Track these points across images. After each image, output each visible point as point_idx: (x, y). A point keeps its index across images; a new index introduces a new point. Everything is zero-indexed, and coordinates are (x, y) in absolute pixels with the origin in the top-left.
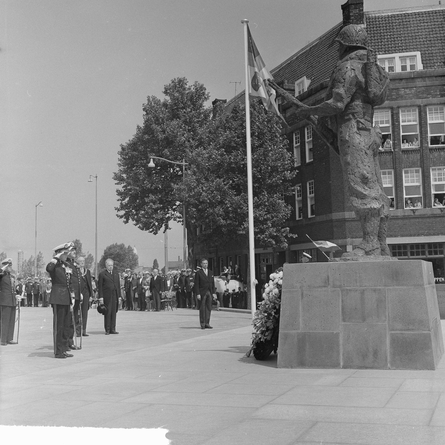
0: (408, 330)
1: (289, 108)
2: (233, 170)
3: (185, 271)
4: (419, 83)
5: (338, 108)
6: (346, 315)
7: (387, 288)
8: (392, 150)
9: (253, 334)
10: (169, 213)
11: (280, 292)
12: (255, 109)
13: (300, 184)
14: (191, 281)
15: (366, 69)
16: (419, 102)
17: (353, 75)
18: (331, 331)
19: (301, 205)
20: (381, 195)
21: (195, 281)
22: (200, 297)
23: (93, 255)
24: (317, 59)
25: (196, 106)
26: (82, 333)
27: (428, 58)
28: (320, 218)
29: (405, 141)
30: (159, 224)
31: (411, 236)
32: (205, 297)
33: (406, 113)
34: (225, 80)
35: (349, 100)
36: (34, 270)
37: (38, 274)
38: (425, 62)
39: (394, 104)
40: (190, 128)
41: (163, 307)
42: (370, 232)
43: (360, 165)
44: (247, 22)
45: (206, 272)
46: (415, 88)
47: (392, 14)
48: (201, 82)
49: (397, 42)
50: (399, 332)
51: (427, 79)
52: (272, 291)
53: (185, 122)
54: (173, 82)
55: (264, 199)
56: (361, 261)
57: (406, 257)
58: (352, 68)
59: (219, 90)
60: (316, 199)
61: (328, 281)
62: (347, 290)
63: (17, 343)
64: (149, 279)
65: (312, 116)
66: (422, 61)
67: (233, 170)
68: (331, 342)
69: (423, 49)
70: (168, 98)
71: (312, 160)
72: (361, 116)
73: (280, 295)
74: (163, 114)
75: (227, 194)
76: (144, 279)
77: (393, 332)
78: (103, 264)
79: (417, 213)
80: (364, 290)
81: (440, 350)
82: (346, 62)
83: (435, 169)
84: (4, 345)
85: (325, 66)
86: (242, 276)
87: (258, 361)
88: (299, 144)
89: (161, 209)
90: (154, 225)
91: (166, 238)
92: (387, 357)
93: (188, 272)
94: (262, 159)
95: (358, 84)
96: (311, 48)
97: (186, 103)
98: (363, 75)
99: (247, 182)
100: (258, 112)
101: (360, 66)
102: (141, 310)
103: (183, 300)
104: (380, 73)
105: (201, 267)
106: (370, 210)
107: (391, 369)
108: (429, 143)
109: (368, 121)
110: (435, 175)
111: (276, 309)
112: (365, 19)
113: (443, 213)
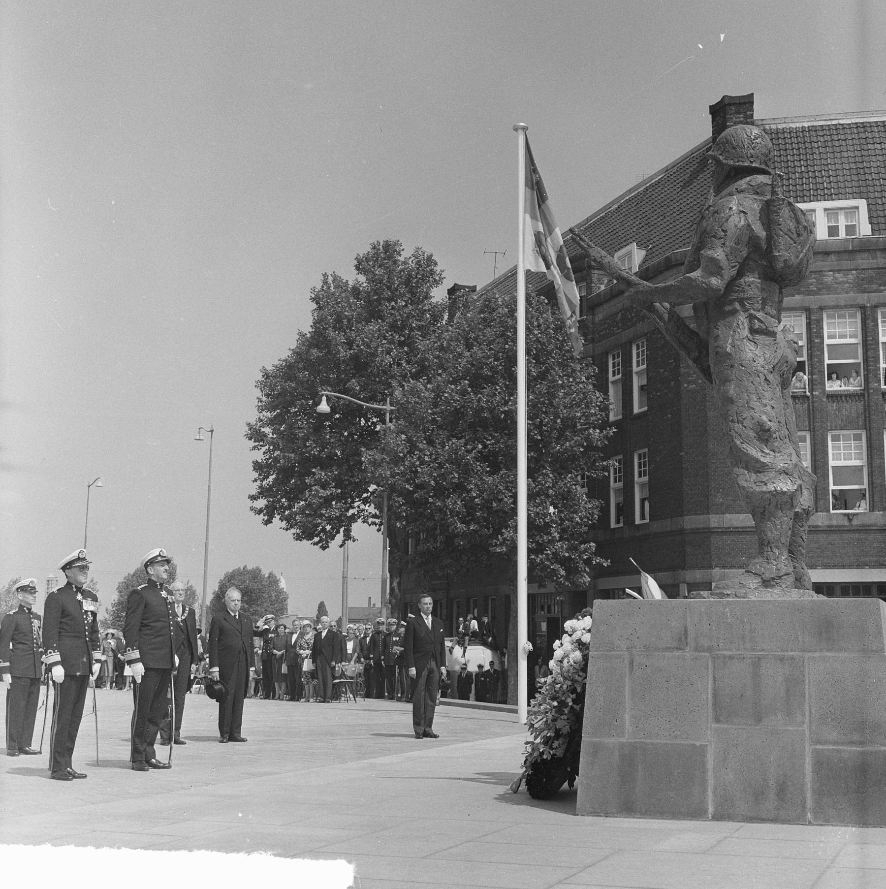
1: (600, 304)
2: (484, 424)
3: (383, 623)
5: (712, 289)
6: (722, 710)
8: (808, 394)
9: (527, 743)
11: (585, 658)
13: (621, 457)
14: (396, 643)
15: (768, 213)
17: (742, 223)
19: (621, 499)
21: (404, 643)
22: (415, 672)
24: (658, 210)
25: (418, 297)
26: (172, 738)
28: (667, 525)
29: (834, 376)
30: (332, 528)
31: (843, 567)
32: (425, 673)
33: (837, 320)
35: (734, 272)
39: (812, 301)
40: (403, 339)
41: (336, 693)
43: (755, 404)
44: (525, 129)
45: (428, 621)
46: (854, 272)
48: (428, 250)
49: (820, 180)
51: (879, 254)
52: (567, 656)
53: (393, 327)
54: (374, 248)
55: (546, 483)
56: (753, 598)
58: (740, 209)
59: (462, 267)
62: (724, 656)
63: (40, 753)
64: (310, 636)
66: (870, 217)
67: (484, 424)
69: (872, 195)
70: (362, 278)
71: (646, 408)
73: (586, 665)
74: (353, 309)
75: (473, 470)
76: (302, 635)
78: (220, 597)
79: (855, 522)
80: (759, 659)
82: (729, 198)
84: (13, 755)
86: (499, 638)
87: (536, 802)
89: (338, 498)
90: (324, 530)
91: (346, 558)
92: (804, 798)
93: (390, 624)
94: (543, 403)
95: (753, 241)
97: (396, 290)
98: (763, 225)
101: (757, 206)
102: (292, 699)
103: (377, 683)
106: (774, 495)
108: (882, 382)
111: (577, 693)
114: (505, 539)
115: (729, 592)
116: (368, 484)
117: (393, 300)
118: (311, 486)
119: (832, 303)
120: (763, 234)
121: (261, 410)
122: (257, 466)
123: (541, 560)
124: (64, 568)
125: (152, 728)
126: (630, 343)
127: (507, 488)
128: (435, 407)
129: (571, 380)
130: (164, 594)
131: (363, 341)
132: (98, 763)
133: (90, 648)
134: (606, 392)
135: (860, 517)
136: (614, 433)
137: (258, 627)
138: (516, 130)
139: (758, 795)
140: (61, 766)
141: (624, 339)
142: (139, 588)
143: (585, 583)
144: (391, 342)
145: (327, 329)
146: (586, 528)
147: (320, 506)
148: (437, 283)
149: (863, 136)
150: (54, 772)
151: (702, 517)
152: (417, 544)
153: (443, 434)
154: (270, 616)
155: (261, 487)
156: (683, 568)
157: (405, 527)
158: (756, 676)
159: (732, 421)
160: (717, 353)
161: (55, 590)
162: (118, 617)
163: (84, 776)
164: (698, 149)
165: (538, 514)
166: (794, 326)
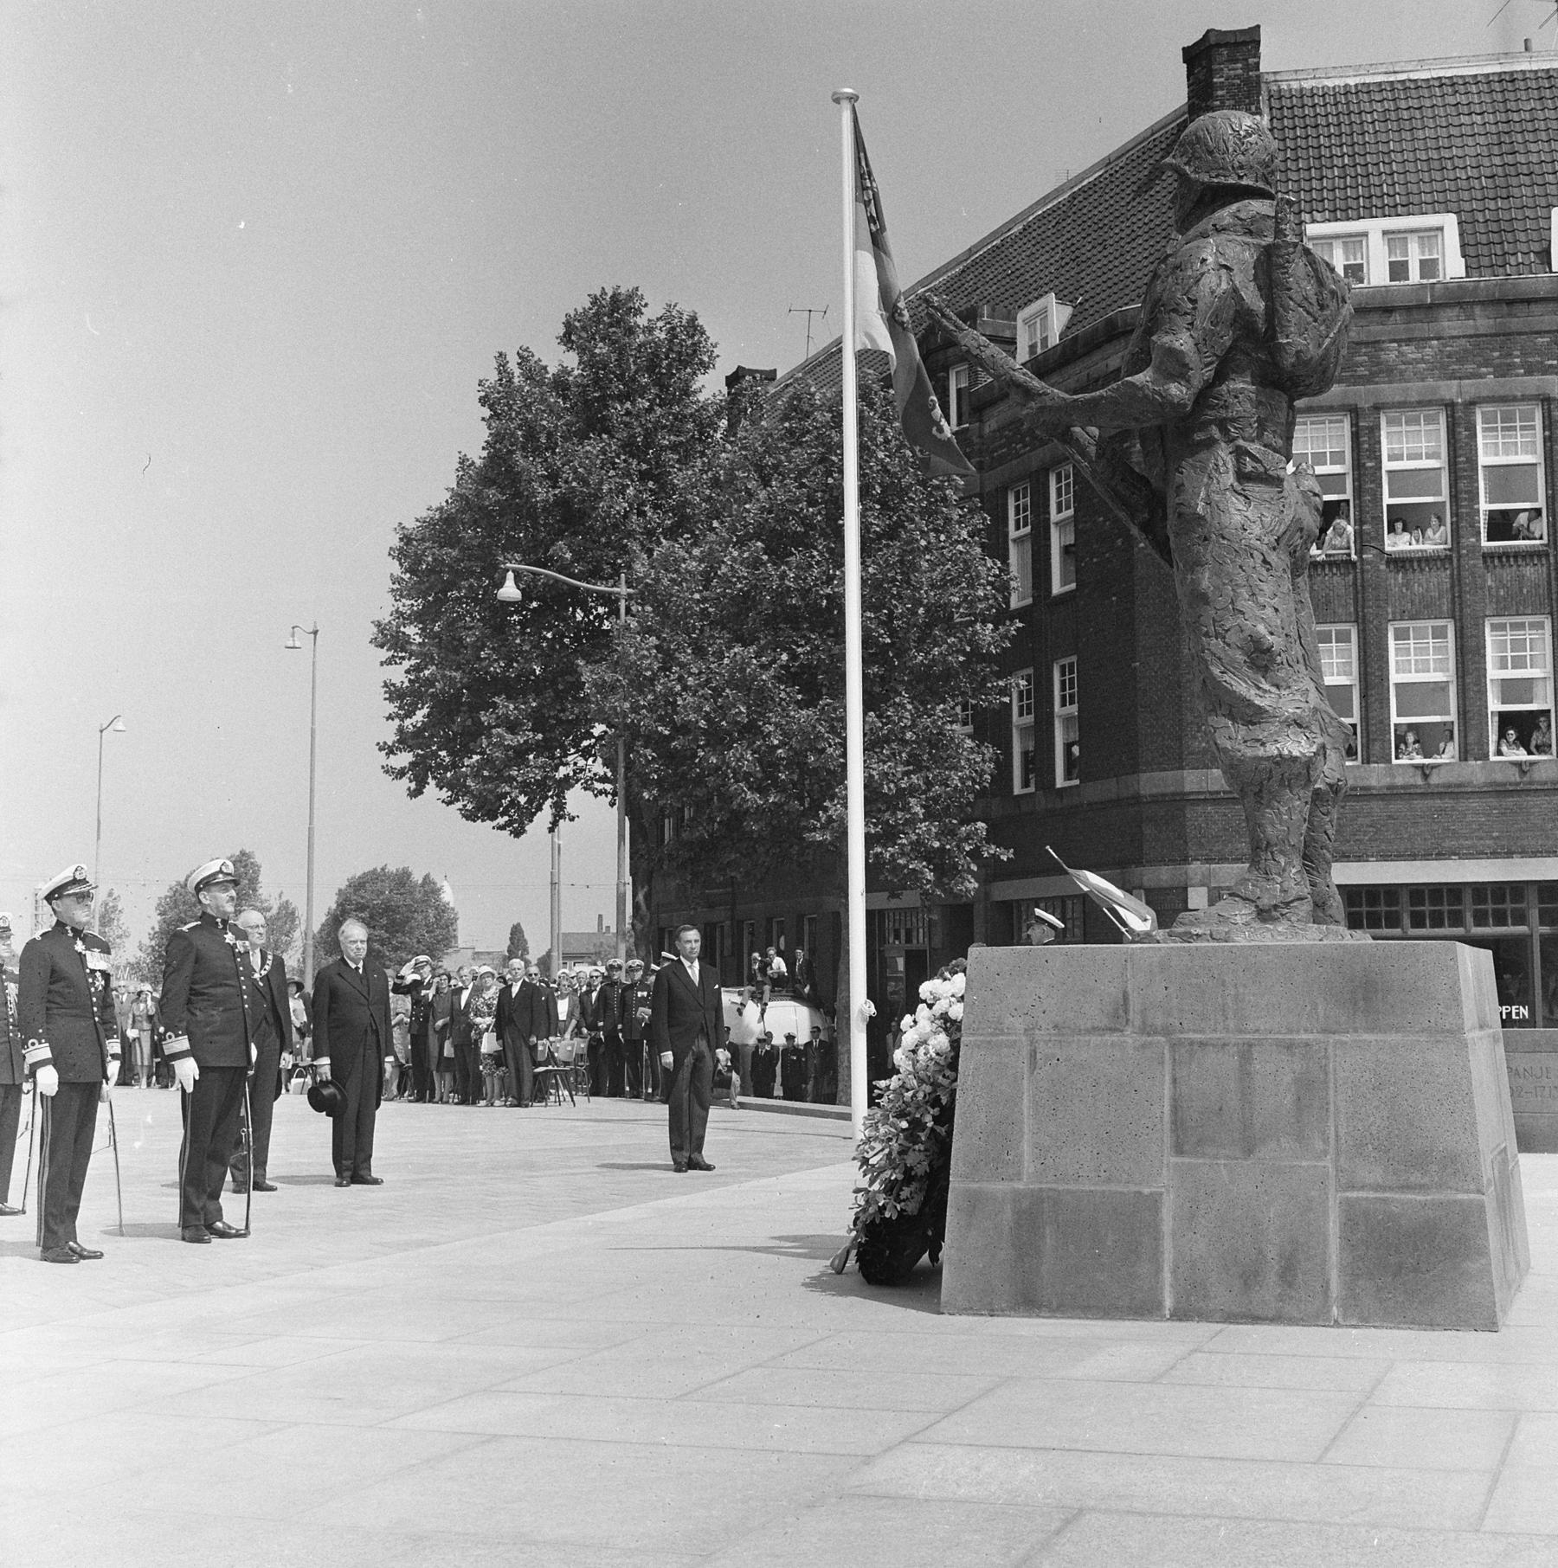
1: (992, 403)
2: (792, 618)
3: (620, 967)
4: (1451, 324)
5: (1171, 403)
6: (1186, 1135)
7: (1333, 1038)
9: (857, 1191)
10: (567, 764)
11: (955, 1045)
12: (871, 405)
13: (1030, 671)
14: (642, 1002)
15: (1269, 268)
16: (1450, 390)
17: (1224, 286)
18: (1133, 1188)
20: (1316, 710)
21: (653, 1002)
26: (254, 1181)
27: (1483, 239)
29: (1399, 526)
30: (530, 802)
31: (1414, 857)
33: (1404, 428)
35: (1209, 373)
38: (1471, 251)
39: (1362, 395)
40: (644, 466)
41: (540, 1090)
43: (1245, 604)
44: (853, 99)
45: (694, 970)
48: (686, 309)
50: (1372, 1195)
51: (1477, 310)
52: (925, 1042)
53: (629, 447)
56: (1241, 941)
57: (1397, 931)
58: (1220, 261)
60: (1085, 725)
61: (1126, 1012)
62: (1192, 1043)
63: (24, 1212)
64: (492, 993)
65: (1077, 429)
66: (1463, 246)
67: (792, 618)
68: (1134, 1221)
69: (1466, 206)
70: (572, 360)
71: (1073, 586)
72: (1251, 432)
73: (956, 1058)
75: (772, 699)
76: (478, 991)
78: (330, 938)
79: (1435, 779)
83: (1502, 627)
86: (819, 987)
87: (874, 1290)
88: (1028, 528)
89: (540, 749)
91: (556, 850)
93: (630, 970)
94: (894, 580)
95: (1242, 317)
96: (1074, 197)
98: (1260, 289)
100: (883, 416)
101: (1249, 256)
102: (463, 1102)
103: (611, 1070)
106: (1277, 763)
108: (1484, 535)
109: (1276, 451)
110: (1501, 646)
112: (1264, 97)
114: (830, 819)
115: (1200, 931)
116: (589, 724)
117: (628, 399)
118: (490, 727)
119: (1397, 398)
120: (1259, 305)
121: (398, 594)
122: (394, 693)
123: (892, 855)
124: (49, 898)
125: (215, 1169)
126: (1044, 471)
127: (832, 730)
128: (706, 588)
129: (943, 537)
130: (229, 938)
131: (575, 472)
132: (121, 1231)
133: (102, 1035)
134: (1005, 559)
135: (1443, 770)
136: (1018, 629)
137: (402, 978)
138: (837, 101)
140: (58, 1238)
141: (1035, 465)
142: (185, 928)
143: (968, 890)
146: (971, 797)
147: (508, 763)
148: (705, 366)
149: (1451, 100)
150: (46, 1248)
152: (677, 829)
153: (721, 638)
154: (422, 958)
155: (400, 730)
156: (1139, 863)
158: (1245, 1074)
160: (1180, 515)
161: (37, 936)
163: (98, 1256)
164: (1162, 125)
165: (887, 774)
166: (1320, 445)
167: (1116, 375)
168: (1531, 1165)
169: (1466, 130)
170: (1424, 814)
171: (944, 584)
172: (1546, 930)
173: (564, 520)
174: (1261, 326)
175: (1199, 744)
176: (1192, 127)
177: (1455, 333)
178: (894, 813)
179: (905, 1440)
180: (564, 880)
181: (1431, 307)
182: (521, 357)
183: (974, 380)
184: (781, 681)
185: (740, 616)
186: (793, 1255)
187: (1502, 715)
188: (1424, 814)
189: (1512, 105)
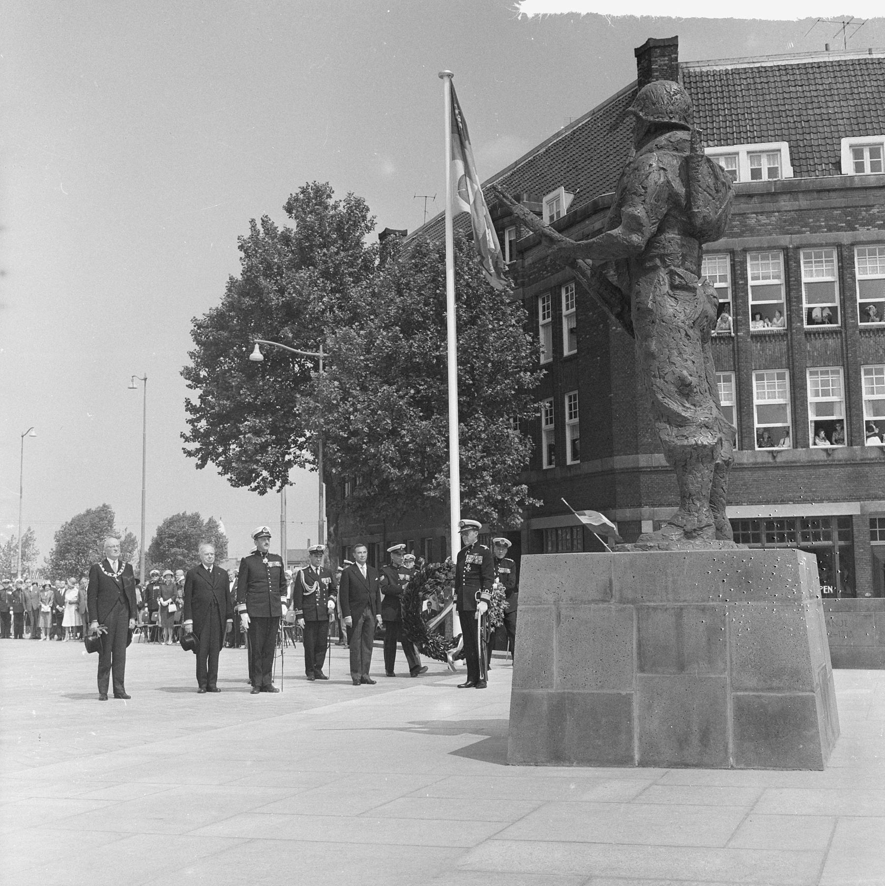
0: (771, 689)
4: (785, 203)
5: (633, 246)
6: (646, 660)
10: (290, 453)
12: (461, 250)
13: (552, 399)
15: (688, 168)
16: (785, 240)
17: (662, 180)
18: (615, 691)
20: (716, 418)
23: (137, 534)
24: (586, 154)
27: (803, 156)
28: (595, 465)
29: (758, 317)
31: (767, 502)
32: (361, 621)
33: (760, 262)
34: (409, 189)
35: (654, 229)
36: (16, 564)
37: (23, 571)
38: (796, 163)
39: (736, 243)
40: (334, 285)
42: (693, 493)
43: (676, 359)
44: (450, 76)
45: (364, 570)
46: (777, 214)
47: (733, 67)
49: (743, 123)
50: (752, 694)
51: (800, 196)
53: (325, 274)
55: (478, 427)
56: (675, 550)
57: (759, 545)
58: (659, 166)
59: (396, 211)
60: (582, 428)
62: (648, 607)
65: (580, 261)
66: (792, 160)
67: (417, 368)
68: (617, 709)
69: (793, 138)
71: (575, 351)
72: (678, 262)
75: (406, 415)
77: (739, 693)
79: (779, 459)
80: (681, 609)
81: (833, 732)
82: (649, 155)
83: (816, 373)
85: (601, 168)
88: (550, 319)
91: (284, 503)
94: (474, 348)
95: (673, 197)
96: (574, 133)
98: (682, 181)
99: (446, 392)
100: (468, 255)
101: (676, 163)
104: (716, 178)
105: (354, 560)
106: (695, 449)
107: (735, 769)
108: (805, 322)
109: (692, 272)
110: (815, 384)
112: (680, 76)
113: (830, 458)
114: (439, 484)
115: (652, 544)
117: (324, 247)
120: (681, 190)
126: (560, 287)
127: (440, 433)
131: (294, 288)
134: (536, 336)
136: (544, 375)
139: (682, 742)
144: (324, 289)
145: (256, 277)
147: (256, 452)
148: (368, 229)
151: (631, 457)
153: (377, 380)
157: (340, 473)
158: (679, 626)
159: (654, 376)
162: (57, 565)
164: (623, 92)
166: (715, 271)
167: (600, 231)
168: (839, 675)
169: (793, 95)
170: (783, 478)
171: (501, 350)
172: (842, 543)
173: (287, 314)
174: (684, 202)
175: (647, 440)
176: (643, 90)
177: (788, 209)
178: (474, 479)
179: (489, 838)
180: (288, 519)
181: (774, 194)
182: (263, 221)
183: (518, 233)
184: (410, 405)
185: (389, 368)
186: (422, 732)
187: (816, 422)
188: (783, 478)
189: (819, 81)
